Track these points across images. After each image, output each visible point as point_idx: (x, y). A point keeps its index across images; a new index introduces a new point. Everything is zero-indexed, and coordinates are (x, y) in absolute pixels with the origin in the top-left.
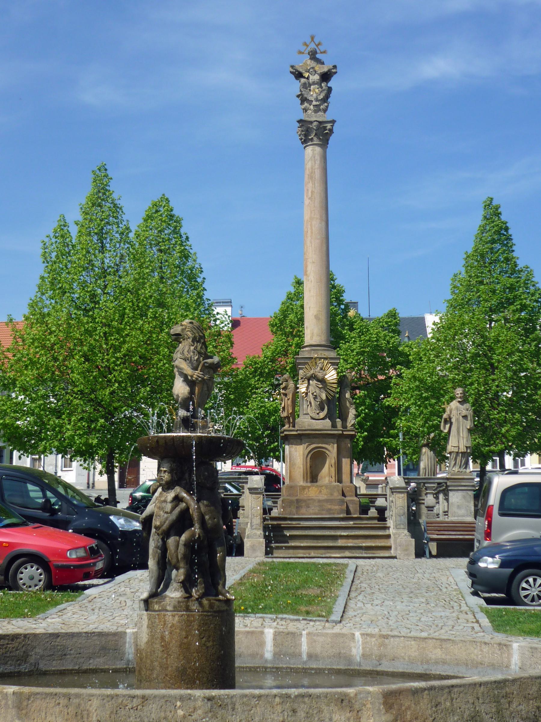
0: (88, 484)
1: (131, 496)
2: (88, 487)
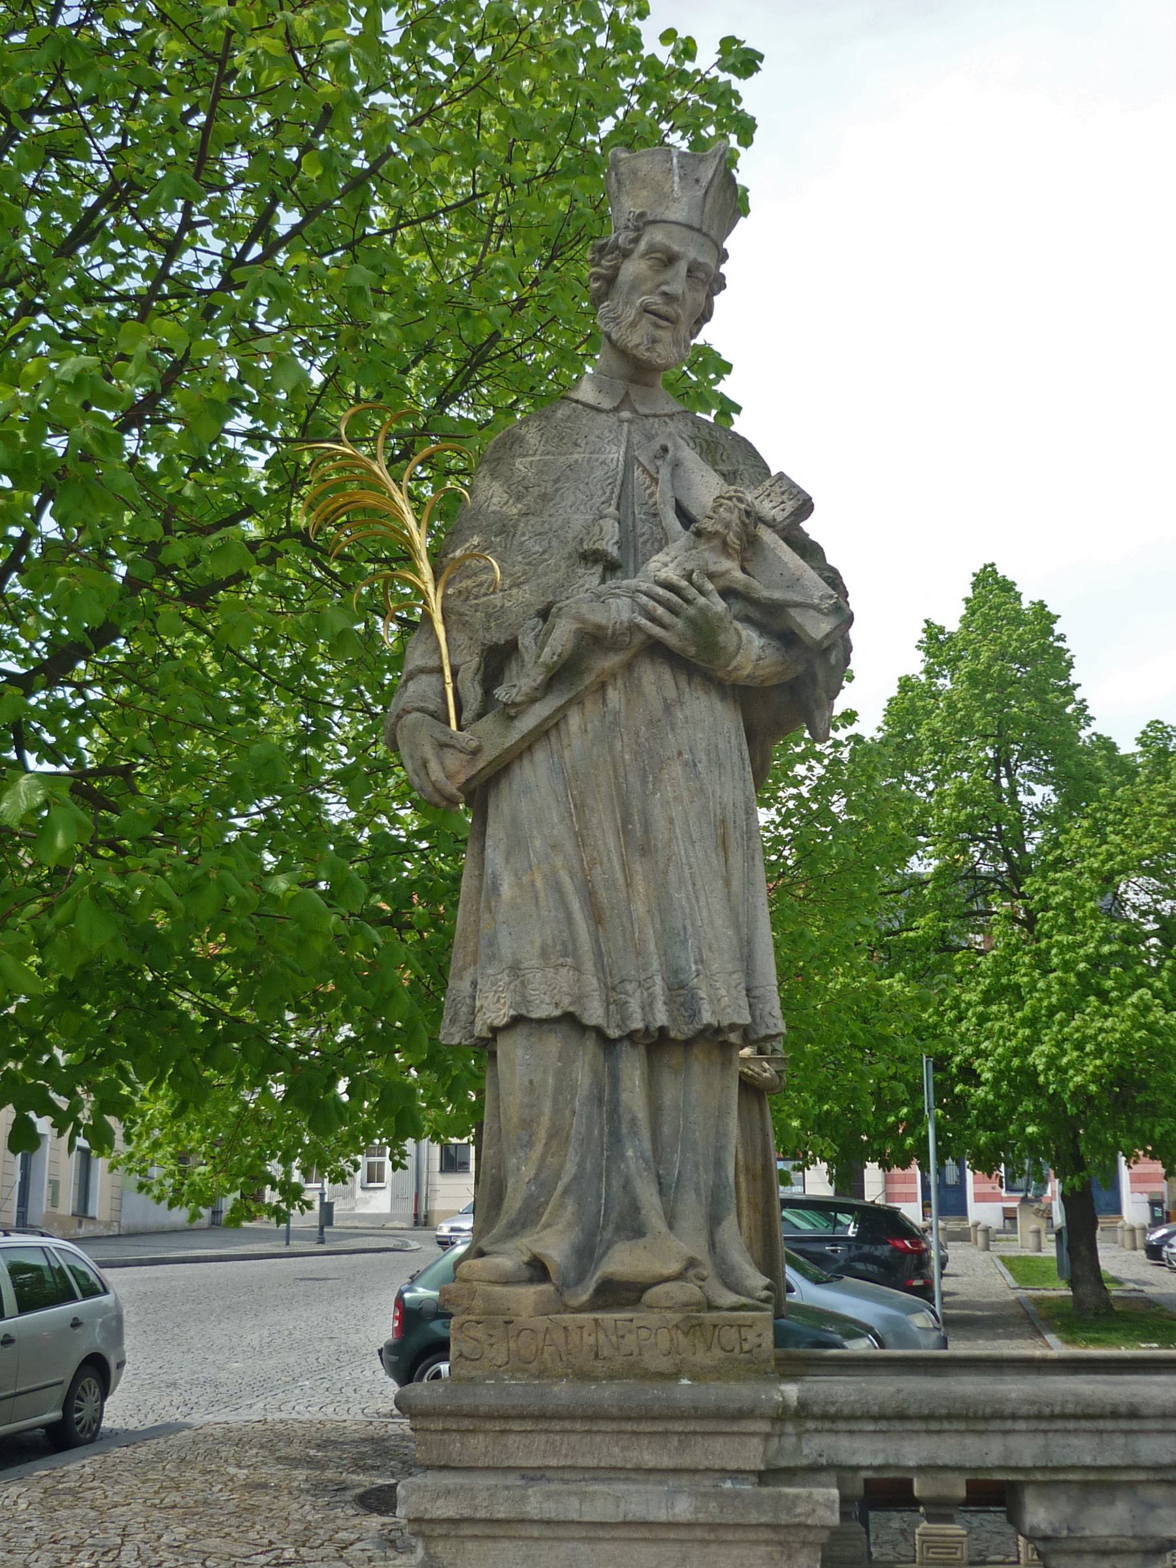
0: (416, 1216)
1: (400, 1302)
2: (416, 1223)
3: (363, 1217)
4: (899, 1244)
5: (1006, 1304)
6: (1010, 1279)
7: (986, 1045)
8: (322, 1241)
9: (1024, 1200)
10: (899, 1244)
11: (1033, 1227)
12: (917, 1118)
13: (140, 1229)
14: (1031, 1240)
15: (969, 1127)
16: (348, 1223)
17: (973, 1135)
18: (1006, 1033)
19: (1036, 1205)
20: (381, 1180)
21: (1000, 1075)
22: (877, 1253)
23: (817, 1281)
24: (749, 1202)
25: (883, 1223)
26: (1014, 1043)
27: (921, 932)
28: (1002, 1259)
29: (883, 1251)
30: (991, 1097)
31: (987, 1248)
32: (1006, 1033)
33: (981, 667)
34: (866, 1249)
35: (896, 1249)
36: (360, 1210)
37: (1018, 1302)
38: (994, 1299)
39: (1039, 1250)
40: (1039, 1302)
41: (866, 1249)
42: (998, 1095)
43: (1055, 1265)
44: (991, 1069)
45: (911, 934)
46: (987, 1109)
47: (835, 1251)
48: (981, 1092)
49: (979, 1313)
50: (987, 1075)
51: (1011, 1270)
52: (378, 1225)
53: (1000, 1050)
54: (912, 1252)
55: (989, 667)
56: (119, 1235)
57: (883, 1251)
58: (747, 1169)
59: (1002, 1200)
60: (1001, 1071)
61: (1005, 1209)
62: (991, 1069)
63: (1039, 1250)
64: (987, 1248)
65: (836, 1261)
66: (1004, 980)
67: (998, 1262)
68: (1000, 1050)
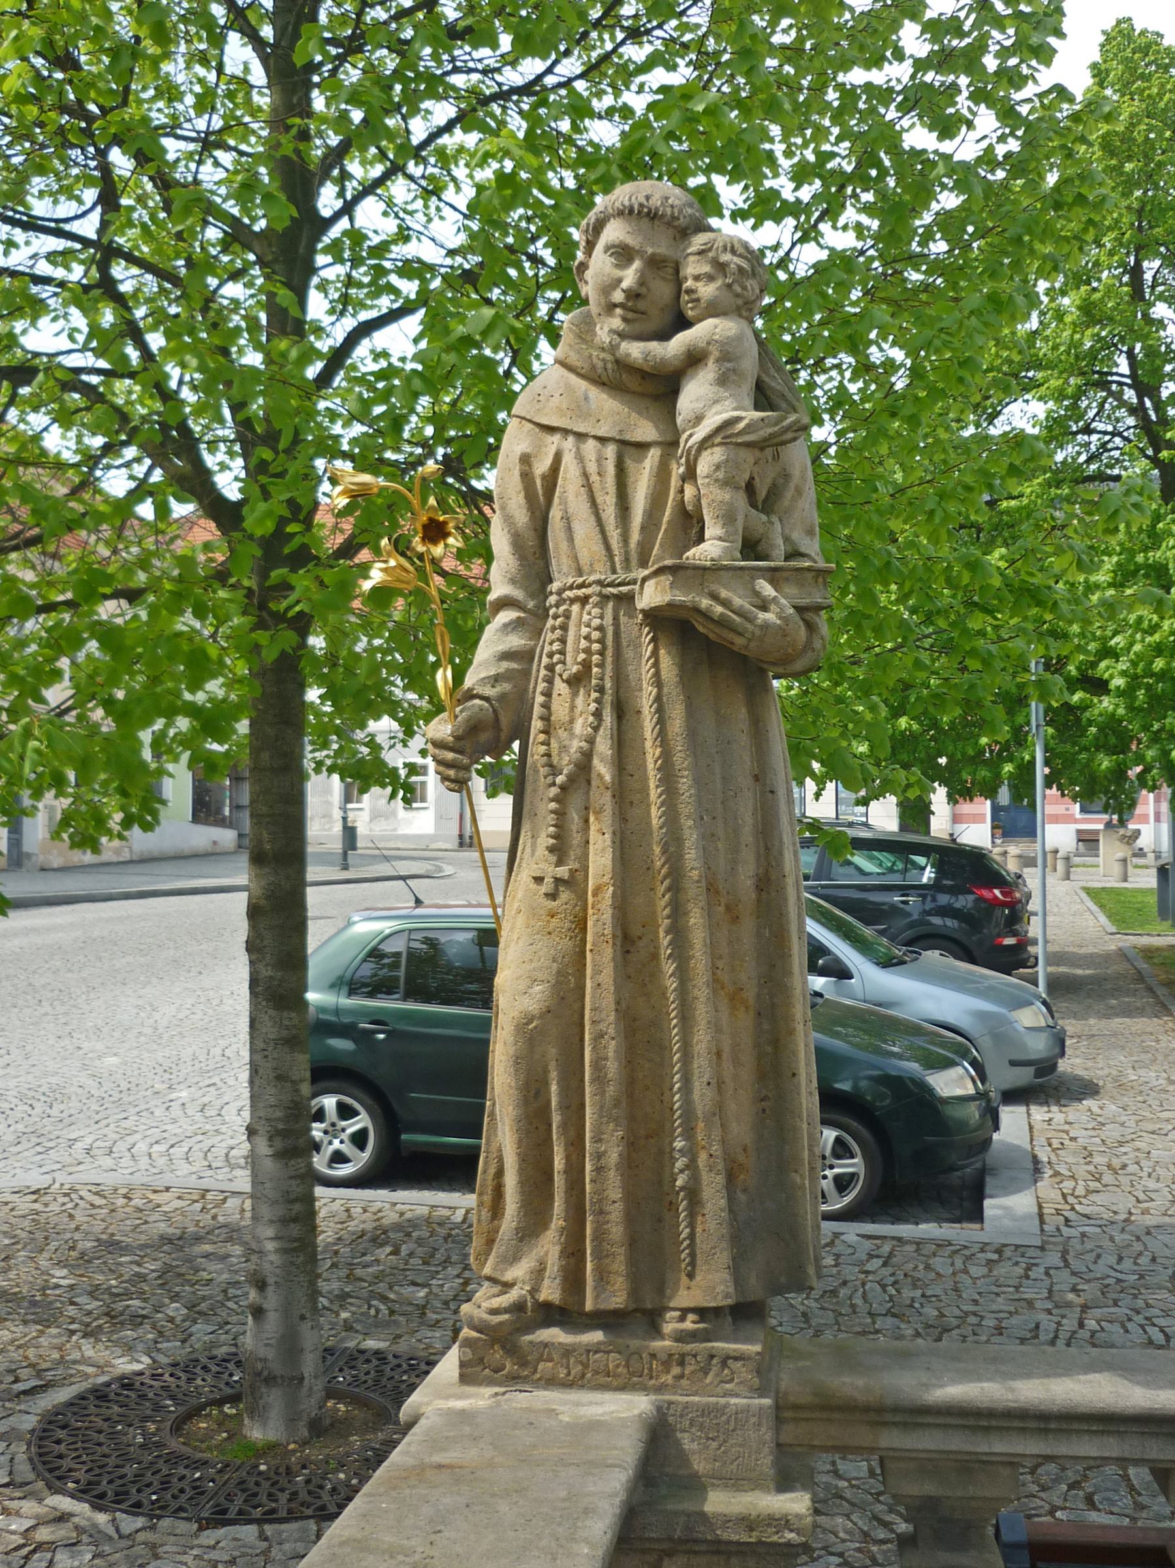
0: (461, 836)
2: (461, 844)
3: (406, 837)
4: (986, 894)
5: (1107, 958)
6: (1103, 919)
7: (1119, 641)
8: (345, 867)
9: (1109, 825)
10: (986, 894)
11: (1120, 855)
12: (1019, 738)
13: (187, 852)
14: (1117, 869)
15: (1086, 749)
16: (392, 845)
17: (1091, 760)
18: (1145, 625)
19: (1122, 831)
20: (423, 800)
21: (1134, 681)
22: (958, 905)
23: (887, 963)
24: (716, 983)
25: (965, 866)
26: (1157, 637)
27: (1025, 501)
28: (1088, 891)
29: (964, 902)
30: (1121, 711)
31: (1067, 877)
32: (1145, 625)
33: (1120, 128)
34: (944, 899)
35: (981, 899)
36: (404, 830)
37: (1122, 954)
38: (1091, 950)
39: (1125, 880)
40: (1149, 953)
41: (944, 899)
42: (1130, 708)
43: (1153, 900)
44: (1123, 673)
45: (1013, 503)
46: (1111, 724)
47: (906, 903)
48: (1106, 703)
49: (1079, 972)
50: (1118, 682)
51: (1102, 906)
52: (422, 850)
53: (1137, 647)
54: (1004, 904)
55: (1131, 126)
56: (131, 862)
57: (964, 902)
58: (711, 889)
59: (1076, 821)
60: (1135, 677)
61: (1079, 832)
62: (1123, 673)
63: (1125, 880)
64: (1067, 877)
65: (909, 915)
66: (1140, 558)
67: (1084, 895)
68: (1137, 647)
